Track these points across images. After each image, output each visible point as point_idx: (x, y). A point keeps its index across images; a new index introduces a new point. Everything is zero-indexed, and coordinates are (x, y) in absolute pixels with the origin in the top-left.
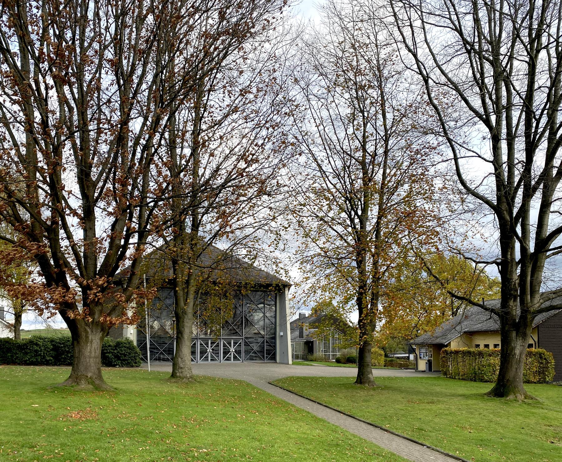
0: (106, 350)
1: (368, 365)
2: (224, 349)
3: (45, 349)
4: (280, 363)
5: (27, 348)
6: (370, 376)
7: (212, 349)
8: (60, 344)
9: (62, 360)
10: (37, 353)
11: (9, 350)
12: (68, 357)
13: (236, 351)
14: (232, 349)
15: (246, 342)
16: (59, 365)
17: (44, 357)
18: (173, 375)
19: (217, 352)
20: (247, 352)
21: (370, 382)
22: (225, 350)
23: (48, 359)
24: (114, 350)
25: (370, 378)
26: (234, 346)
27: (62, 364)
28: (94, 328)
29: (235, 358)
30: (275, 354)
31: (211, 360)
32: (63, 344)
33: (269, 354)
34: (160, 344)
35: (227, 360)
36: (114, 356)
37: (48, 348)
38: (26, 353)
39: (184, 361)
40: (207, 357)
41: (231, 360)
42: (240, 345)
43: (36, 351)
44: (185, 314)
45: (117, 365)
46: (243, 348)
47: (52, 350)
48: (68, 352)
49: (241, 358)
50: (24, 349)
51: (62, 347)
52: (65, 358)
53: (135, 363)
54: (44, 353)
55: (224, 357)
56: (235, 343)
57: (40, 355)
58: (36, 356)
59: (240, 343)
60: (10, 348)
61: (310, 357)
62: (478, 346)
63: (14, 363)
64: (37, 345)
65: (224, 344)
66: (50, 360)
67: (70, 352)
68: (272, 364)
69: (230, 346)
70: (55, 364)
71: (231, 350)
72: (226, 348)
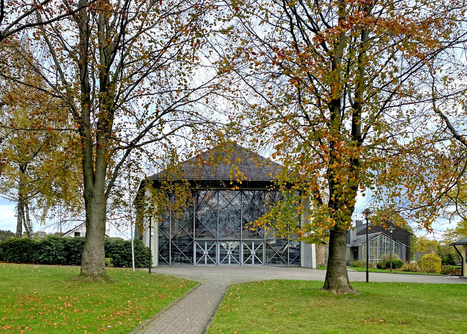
0: (114, 250)
1: (339, 263)
2: (244, 252)
3: (57, 249)
4: (304, 267)
5: (42, 249)
6: (342, 279)
7: (233, 252)
8: (70, 244)
9: (73, 260)
10: (49, 252)
11: (26, 250)
12: (78, 256)
13: (257, 254)
14: (253, 252)
15: (267, 245)
16: (71, 265)
17: (56, 257)
18: (328, 286)
19: (237, 254)
20: (268, 255)
21: (340, 286)
22: (245, 253)
23: (60, 258)
24: (121, 250)
25: (340, 281)
26: (255, 249)
27: (73, 264)
28: (334, 258)
29: (256, 261)
30: (299, 257)
31: (231, 262)
32: (73, 244)
33: (293, 258)
34: (180, 246)
35: (247, 263)
36: (121, 256)
37: (60, 248)
38: (41, 253)
39: (91, 256)
40: (227, 260)
41: (251, 263)
42: (261, 248)
43: (49, 251)
44: (92, 196)
45: (123, 265)
46: (264, 251)
47: (64, 250)
48: (78, 252)
49: (262, 261)
50: (39, 249)
51: (72, 247)
52: (75, 258)
53: (144, 264)
54: (56, 253)
55: (244, 260)
56: (256, 246)
57: (52, 255)
58: (48, 255)
59: (262, 246)
60: (27, 248)
61: (355, 263)
62: (365, 96)
63: (28, 261)
64: (50, 245)
65: (244, 246)
66: (62, 259)
67: (80, 252)
68: (294, 268)
69: (251, 249)
70: (68, 264)
71: (251, 253)
72: (247, 250)
